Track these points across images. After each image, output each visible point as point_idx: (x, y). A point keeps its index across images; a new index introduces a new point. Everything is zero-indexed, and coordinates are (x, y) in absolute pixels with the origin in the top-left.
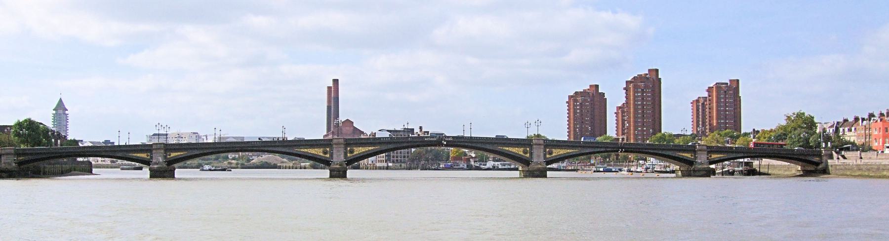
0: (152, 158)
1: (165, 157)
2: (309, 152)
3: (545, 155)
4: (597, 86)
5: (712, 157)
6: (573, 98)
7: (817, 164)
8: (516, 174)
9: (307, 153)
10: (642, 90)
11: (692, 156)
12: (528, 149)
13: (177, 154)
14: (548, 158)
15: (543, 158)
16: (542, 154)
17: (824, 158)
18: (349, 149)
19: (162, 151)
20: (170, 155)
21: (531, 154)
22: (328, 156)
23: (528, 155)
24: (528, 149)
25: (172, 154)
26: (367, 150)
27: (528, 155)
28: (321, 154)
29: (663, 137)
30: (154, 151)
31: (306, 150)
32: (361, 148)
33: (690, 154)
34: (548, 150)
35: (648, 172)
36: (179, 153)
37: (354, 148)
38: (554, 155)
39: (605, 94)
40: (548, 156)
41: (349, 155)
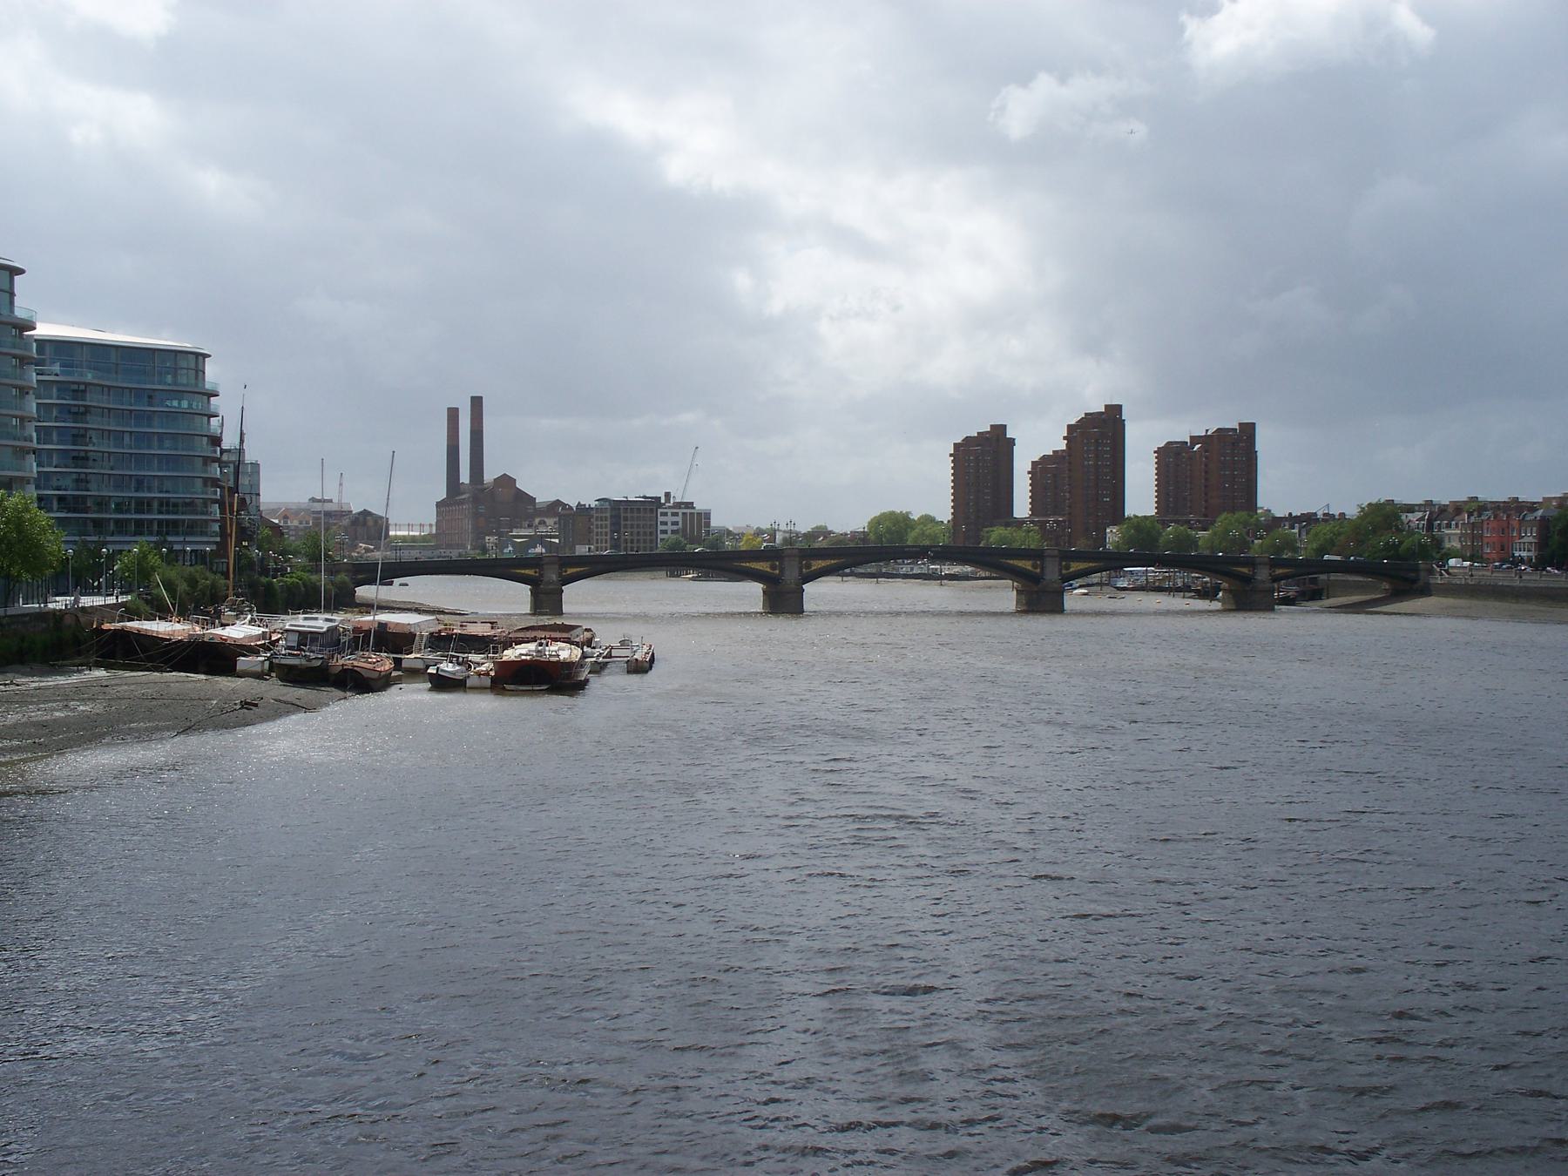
0: (541, 575)
1: (560, 575)
3: (1060, 570)
4: (1004, 427)
5: (568, 573)
6: (1159, 451)
7: (1414, 581)
8: (1217, 605)
10: (1097, 441)
11: (536, 572)
12: (1038, 562)
13: (574, 570)
14: (1065, 575)
15: (1057, 574)
16: (1057, 569)
17: (1423, 574)
19: (557, 567)
20: (566, 572)
21: (1042, 569)
23: (1038, 570)
24: (777, 563)
25: (813, 562)
27: (1038, 570)
29: (395, 547)
30: (545, 567)
31: (748, 564)
33: (533, 570)
34: (1064, 563)
35: (490, 623)
36: (578, 569)
39: (1016, 441)
40: (1064, 572)
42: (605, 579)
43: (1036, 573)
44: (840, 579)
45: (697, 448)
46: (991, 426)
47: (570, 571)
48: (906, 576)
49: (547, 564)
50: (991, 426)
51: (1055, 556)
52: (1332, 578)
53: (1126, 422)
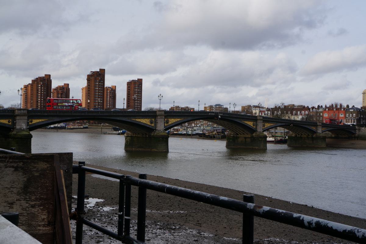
0: (14, 124)
1: (28, 124)
2: (141, 121)
9: (140, 122)
11: (9, 122)
12: (153, 120)
13: (38, 121)
18: (166, 120)
19: (26, 118)
22: (153, 125)
26: (176, 121)
27: (153, 125)
28: (149, 124)
31: (139, 120)
32: (173, 119)
33: (7, 120)
37: (169, 119)
38: (170, 123)
41: (165, 124)
42: (35, 131)
43: (12, 121)
44: (56, 130)
45: (174, 102)
46: (64, 84)
47: (35, 121)
48: (187, 135)
49: (18, 115)
50: (64, 84)
51: (261, 120)
52: (125, 202)
53: (52, 81)
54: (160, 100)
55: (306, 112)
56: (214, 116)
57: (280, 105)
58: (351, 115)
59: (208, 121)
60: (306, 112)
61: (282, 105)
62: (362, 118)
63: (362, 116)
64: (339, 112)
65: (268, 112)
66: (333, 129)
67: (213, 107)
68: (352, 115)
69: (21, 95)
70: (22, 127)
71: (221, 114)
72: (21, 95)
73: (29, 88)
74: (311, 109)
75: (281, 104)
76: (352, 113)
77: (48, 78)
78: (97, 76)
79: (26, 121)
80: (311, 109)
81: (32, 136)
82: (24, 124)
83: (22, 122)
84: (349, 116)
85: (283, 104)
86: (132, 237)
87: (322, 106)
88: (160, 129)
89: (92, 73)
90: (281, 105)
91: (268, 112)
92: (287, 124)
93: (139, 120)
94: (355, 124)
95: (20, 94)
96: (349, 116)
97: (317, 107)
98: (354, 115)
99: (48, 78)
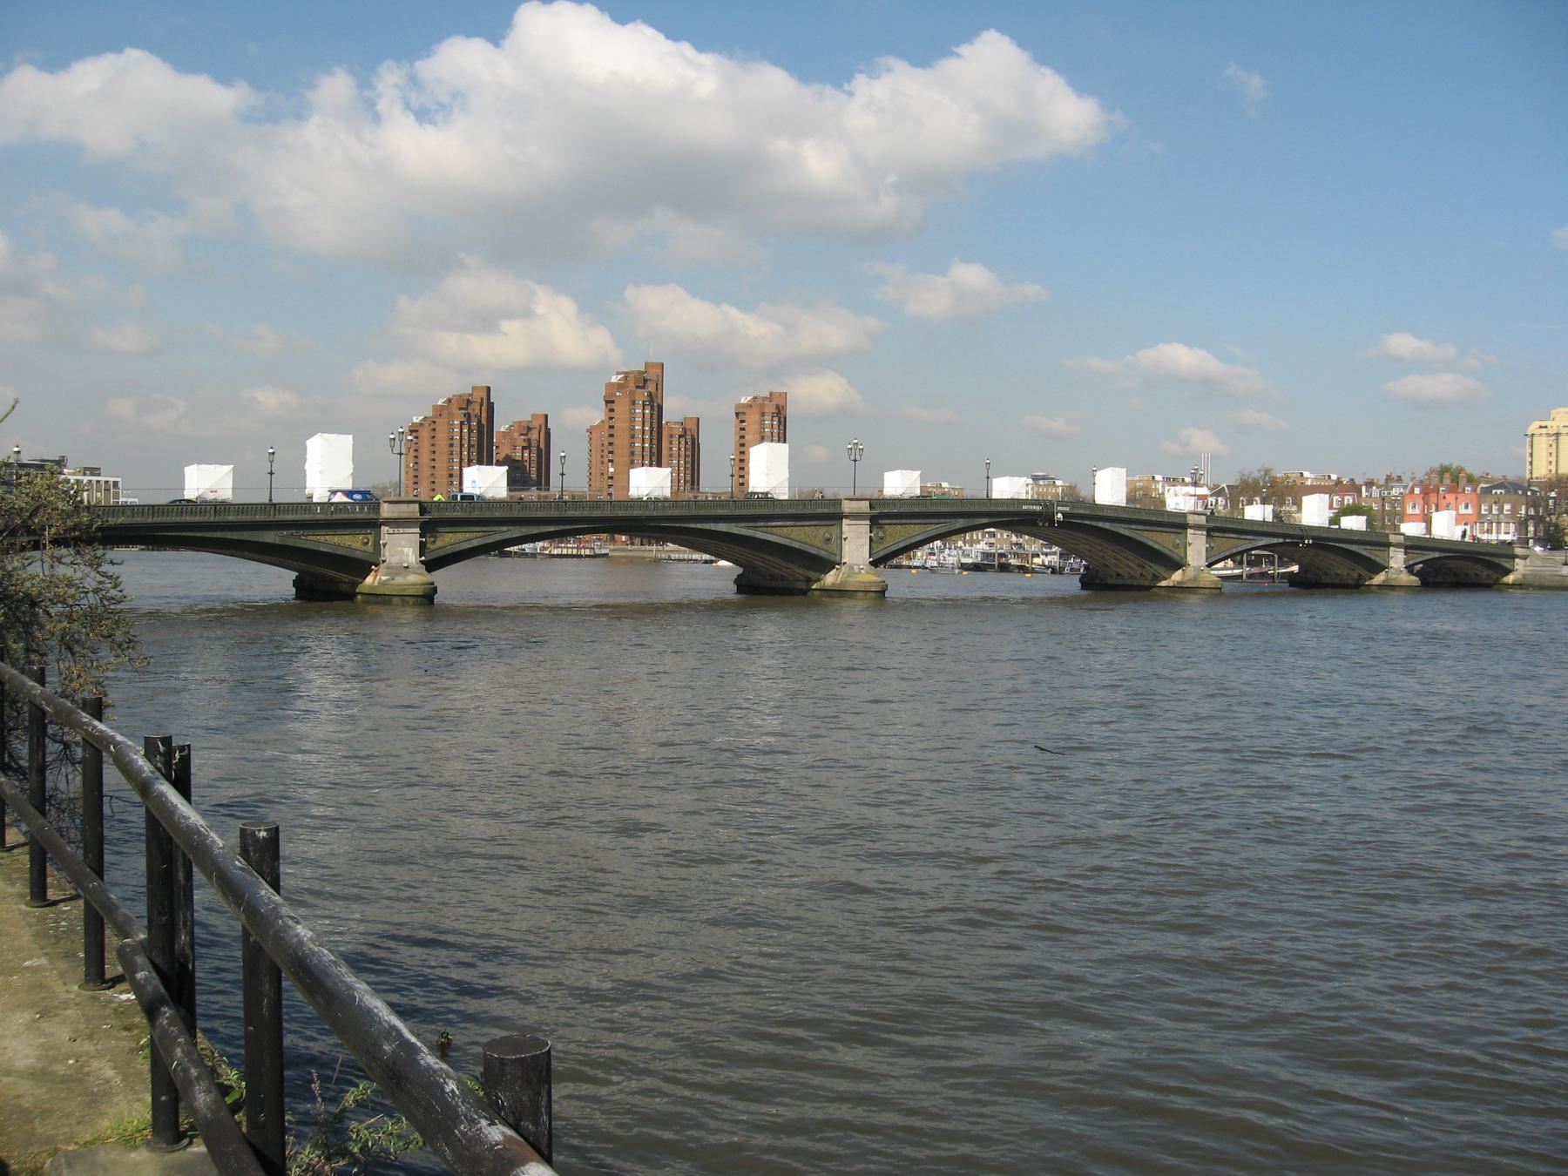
1: (423, 548)
54: (855, 461)
55: (1346, 498)
56: (1040, 514)
57: (1257, 475)
58: (1495, 507)
59: (1013, 531)
60: (1346, 498)
61: (1266, 474)
62: (1532, 517)
63: (1532, 512)
64: (1457, 498)
65: (1217, 500)
66: (1443, 555)
67: (1158, 482)
68: (1501, 510)
69: (400, 454)
70: (405, 558)
71: (1064, 509)
72: (400, 454)
73: (425, 433)
74: (1364, 488)
75: (1259, 471)
76: (1502, 499)
77: (482, 399)
78: (637, 387)
79: (417, 538)
80: (1364, 488)
81: (736, 582)
82: (411, 550)
83: (403, 543)
84: (1490, 510)
85: (1267, 472)
86: (303, 931)
87: (1399, 479)
88: (854, 562)
89: (620, 377)
90: (1263, 473)
91: (1217, 500)
92: (1288, 540)
93: (336, 539)
94: (1508, 538)
95: (397, 450)
96: (1490, 510)
97: (1382, 482)
98: (1507, 507)
99: (482, 399)
